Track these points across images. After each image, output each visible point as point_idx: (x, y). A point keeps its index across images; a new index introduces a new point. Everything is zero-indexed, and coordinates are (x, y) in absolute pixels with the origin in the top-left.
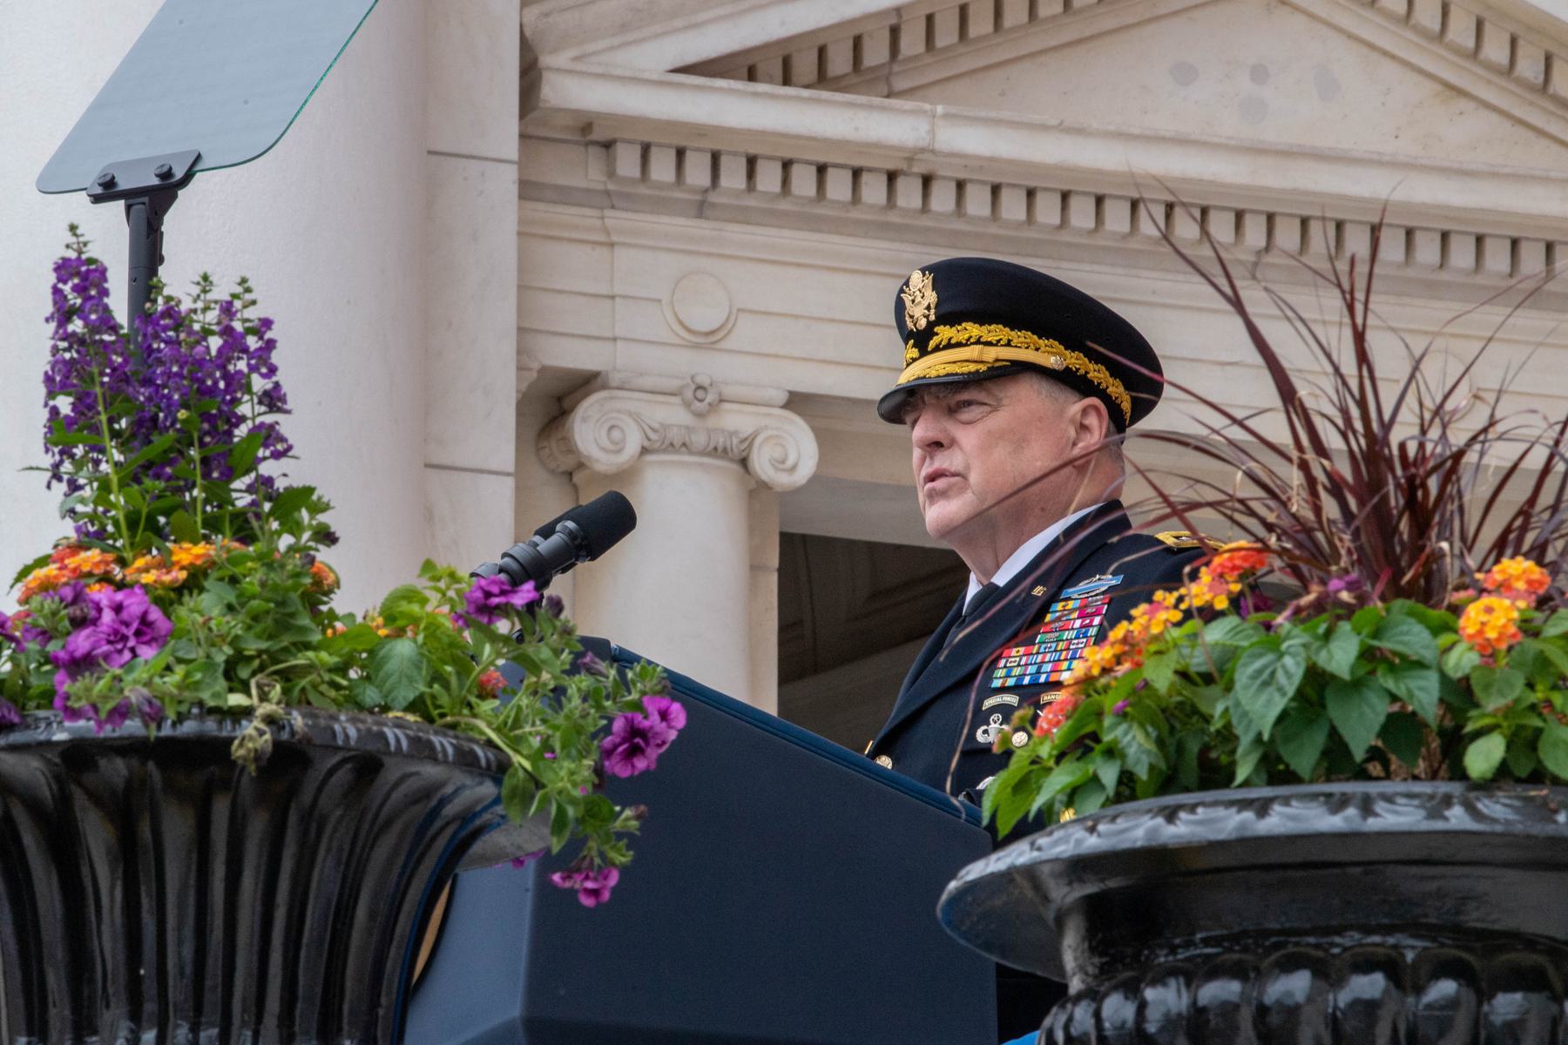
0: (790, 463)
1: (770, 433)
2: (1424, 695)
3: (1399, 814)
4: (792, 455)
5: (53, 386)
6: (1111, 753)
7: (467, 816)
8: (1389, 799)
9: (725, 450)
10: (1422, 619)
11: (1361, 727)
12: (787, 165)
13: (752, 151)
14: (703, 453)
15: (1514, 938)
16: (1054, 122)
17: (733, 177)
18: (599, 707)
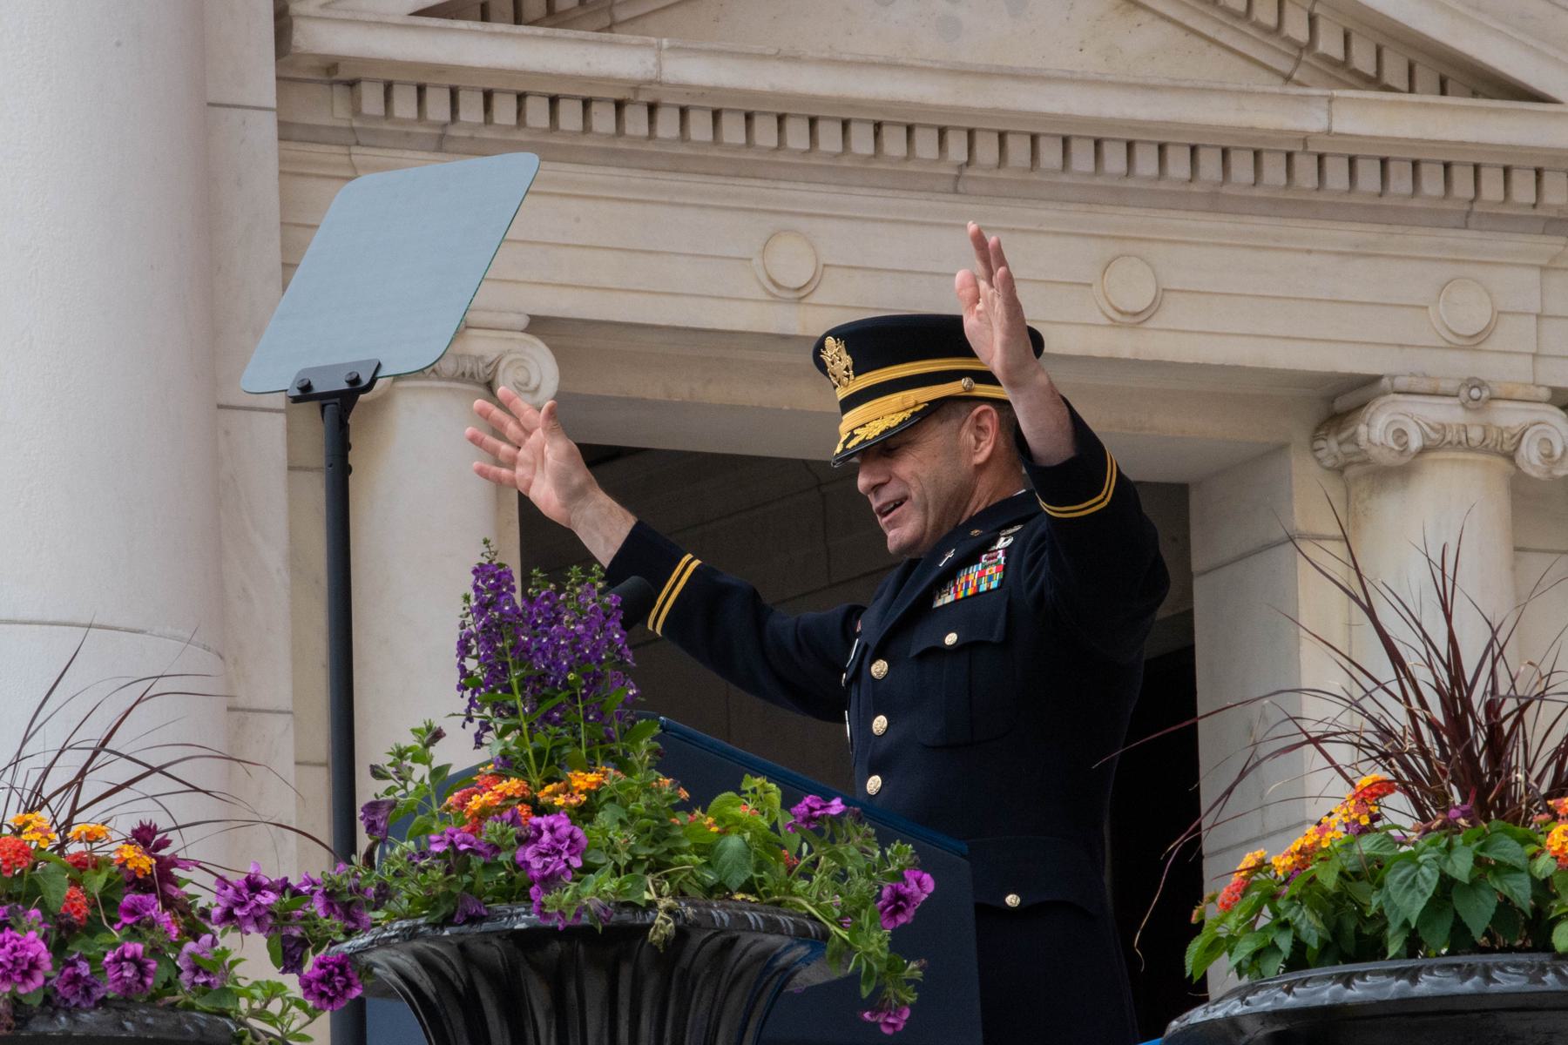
0: (533, 384)
1: (512, 357)
2: (1522, 893)
3: (1509, 980)
5: (464, 649)
7: (785, 969)
9: (472, 375)
10: (1513, 836)
11: (1479, 915)
12: (521, 97)
13: (488, 86)
14: (452, 378)
16: (773, 51)
17: (471, 111)
18: (870, 877)
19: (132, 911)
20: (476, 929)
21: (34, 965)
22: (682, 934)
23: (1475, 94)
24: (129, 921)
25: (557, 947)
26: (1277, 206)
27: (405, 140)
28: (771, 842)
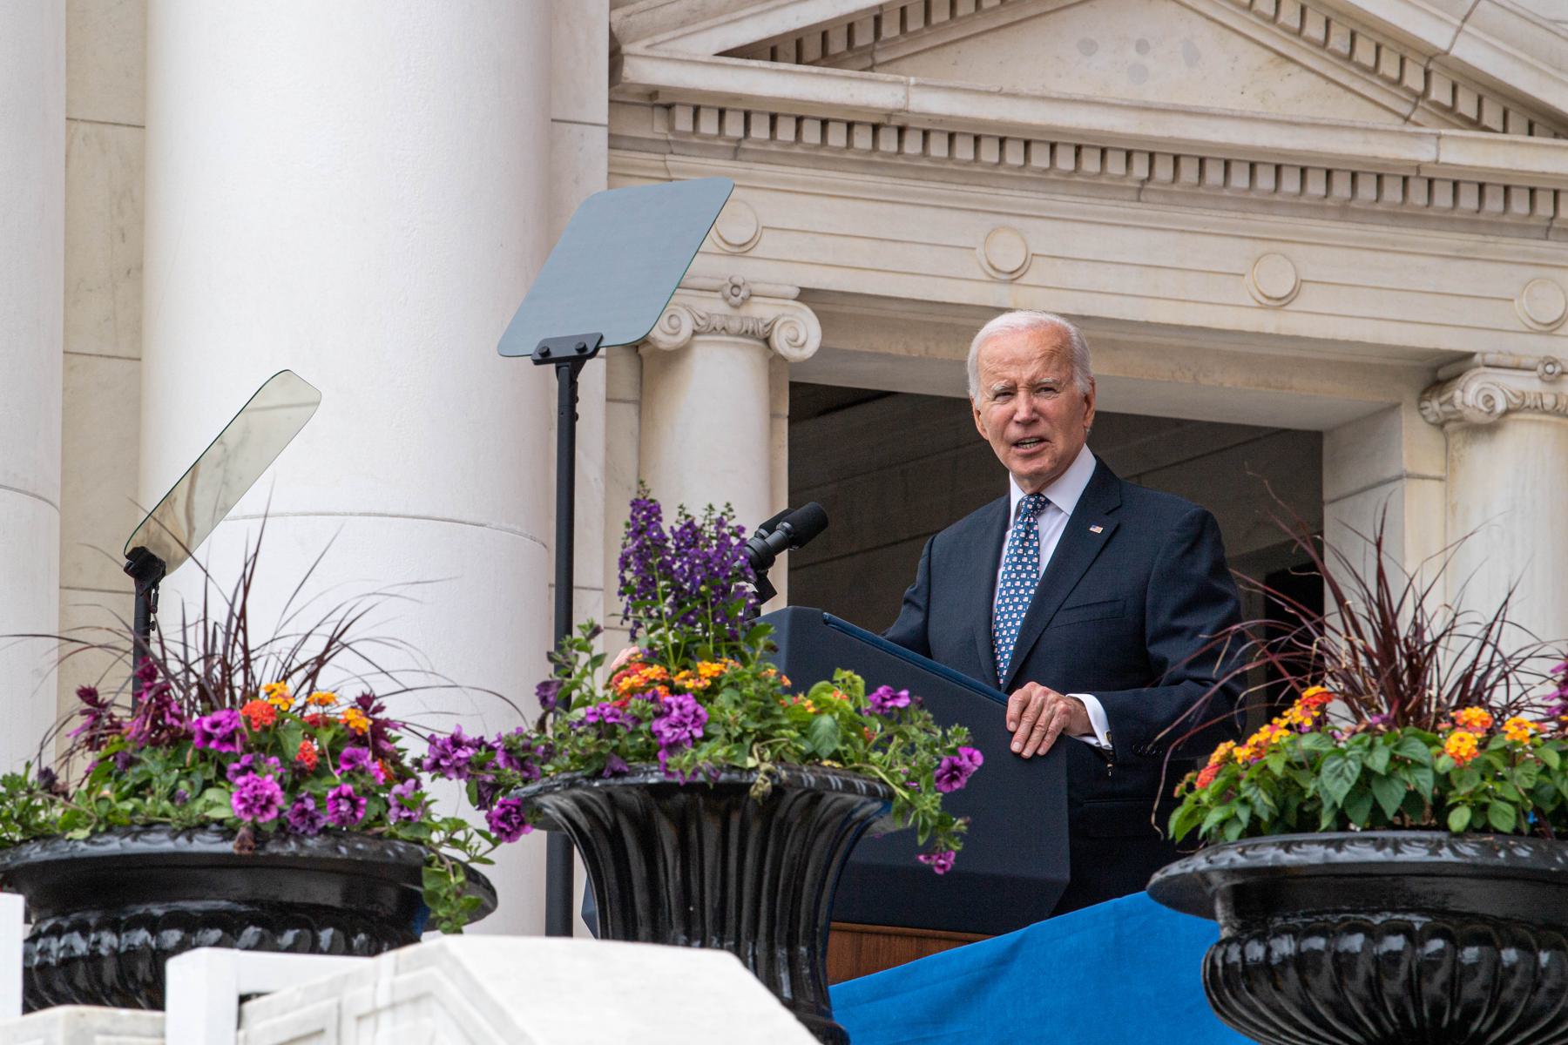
0: (800, 341)
2: (1425, 783)
3: (1415, 854)
4: (802, 336)
5: (624, 563)
6: (1245, 802)
7: (862, 820)
8: (1408, 842)
11: (1391, 799)
14: (739, 335)
15: (1474, 916)
18: (932, 752)
19: (349, 761)
20: (620, 782)
21: (270, 800)
22: (778, 791)
23: (1556, 136)
24: (346, 767)
25: (682, 797)
26: (1396, 216)
27: (707, 148)
28: (852, 724)
